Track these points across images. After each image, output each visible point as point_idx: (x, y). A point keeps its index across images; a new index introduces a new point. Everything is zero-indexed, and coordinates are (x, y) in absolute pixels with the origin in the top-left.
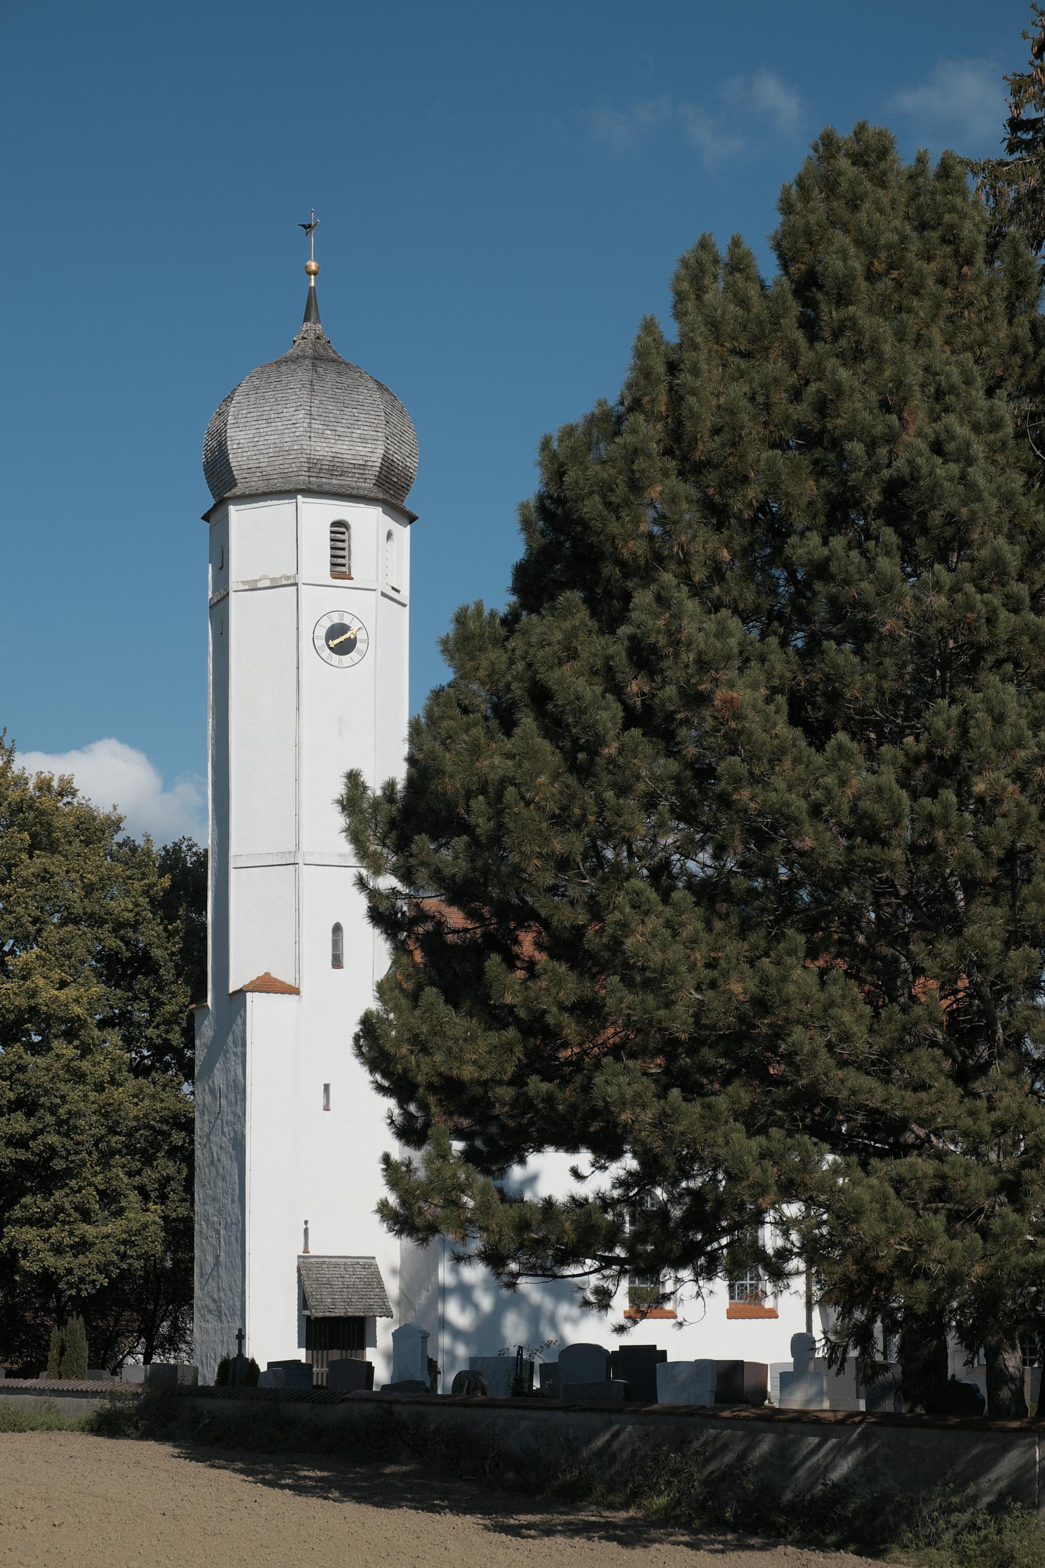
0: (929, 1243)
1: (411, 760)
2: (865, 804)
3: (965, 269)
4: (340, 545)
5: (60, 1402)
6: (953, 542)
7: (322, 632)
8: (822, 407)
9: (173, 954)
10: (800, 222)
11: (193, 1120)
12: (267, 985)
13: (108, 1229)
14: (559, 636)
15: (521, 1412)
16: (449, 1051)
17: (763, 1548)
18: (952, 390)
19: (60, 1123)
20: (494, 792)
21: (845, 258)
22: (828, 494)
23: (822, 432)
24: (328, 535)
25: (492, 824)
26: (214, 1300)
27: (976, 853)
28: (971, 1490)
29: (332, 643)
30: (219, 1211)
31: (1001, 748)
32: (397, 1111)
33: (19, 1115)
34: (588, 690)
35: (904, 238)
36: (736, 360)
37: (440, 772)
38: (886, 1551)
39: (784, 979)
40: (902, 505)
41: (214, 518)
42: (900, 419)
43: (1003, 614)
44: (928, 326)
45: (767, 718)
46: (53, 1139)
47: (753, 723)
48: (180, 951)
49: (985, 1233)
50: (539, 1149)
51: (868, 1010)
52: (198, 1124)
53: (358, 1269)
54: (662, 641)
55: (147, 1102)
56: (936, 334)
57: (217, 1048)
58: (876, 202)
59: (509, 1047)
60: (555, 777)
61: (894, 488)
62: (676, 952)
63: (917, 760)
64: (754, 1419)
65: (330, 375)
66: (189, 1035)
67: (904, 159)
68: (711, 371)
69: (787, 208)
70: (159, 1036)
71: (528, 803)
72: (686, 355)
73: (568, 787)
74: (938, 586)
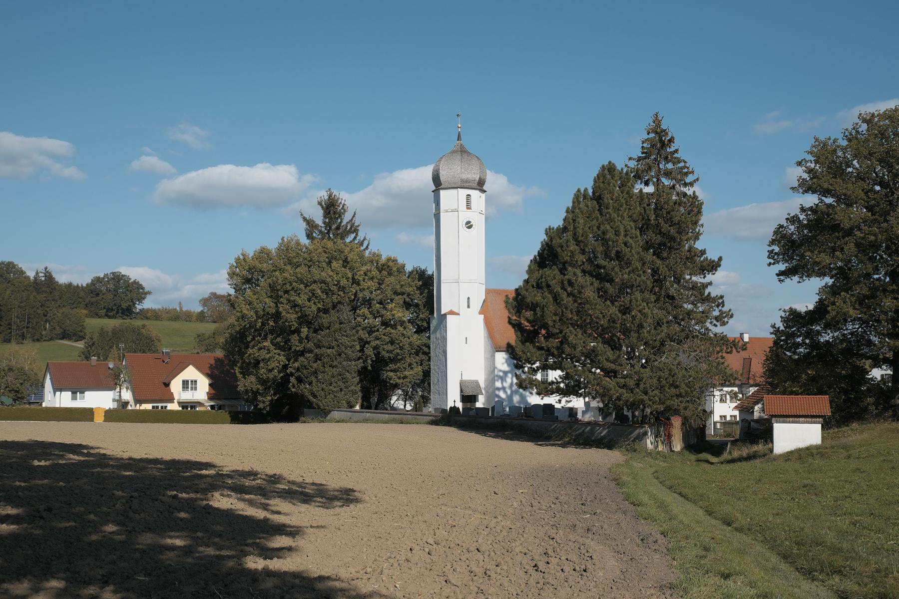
6: (629, 263)
8: (604, 233)
12: (452, 313)
40: (619, 256)
46: (398, 351)
61: (617, 252)
65: (465, 156)
69: (595, 181)
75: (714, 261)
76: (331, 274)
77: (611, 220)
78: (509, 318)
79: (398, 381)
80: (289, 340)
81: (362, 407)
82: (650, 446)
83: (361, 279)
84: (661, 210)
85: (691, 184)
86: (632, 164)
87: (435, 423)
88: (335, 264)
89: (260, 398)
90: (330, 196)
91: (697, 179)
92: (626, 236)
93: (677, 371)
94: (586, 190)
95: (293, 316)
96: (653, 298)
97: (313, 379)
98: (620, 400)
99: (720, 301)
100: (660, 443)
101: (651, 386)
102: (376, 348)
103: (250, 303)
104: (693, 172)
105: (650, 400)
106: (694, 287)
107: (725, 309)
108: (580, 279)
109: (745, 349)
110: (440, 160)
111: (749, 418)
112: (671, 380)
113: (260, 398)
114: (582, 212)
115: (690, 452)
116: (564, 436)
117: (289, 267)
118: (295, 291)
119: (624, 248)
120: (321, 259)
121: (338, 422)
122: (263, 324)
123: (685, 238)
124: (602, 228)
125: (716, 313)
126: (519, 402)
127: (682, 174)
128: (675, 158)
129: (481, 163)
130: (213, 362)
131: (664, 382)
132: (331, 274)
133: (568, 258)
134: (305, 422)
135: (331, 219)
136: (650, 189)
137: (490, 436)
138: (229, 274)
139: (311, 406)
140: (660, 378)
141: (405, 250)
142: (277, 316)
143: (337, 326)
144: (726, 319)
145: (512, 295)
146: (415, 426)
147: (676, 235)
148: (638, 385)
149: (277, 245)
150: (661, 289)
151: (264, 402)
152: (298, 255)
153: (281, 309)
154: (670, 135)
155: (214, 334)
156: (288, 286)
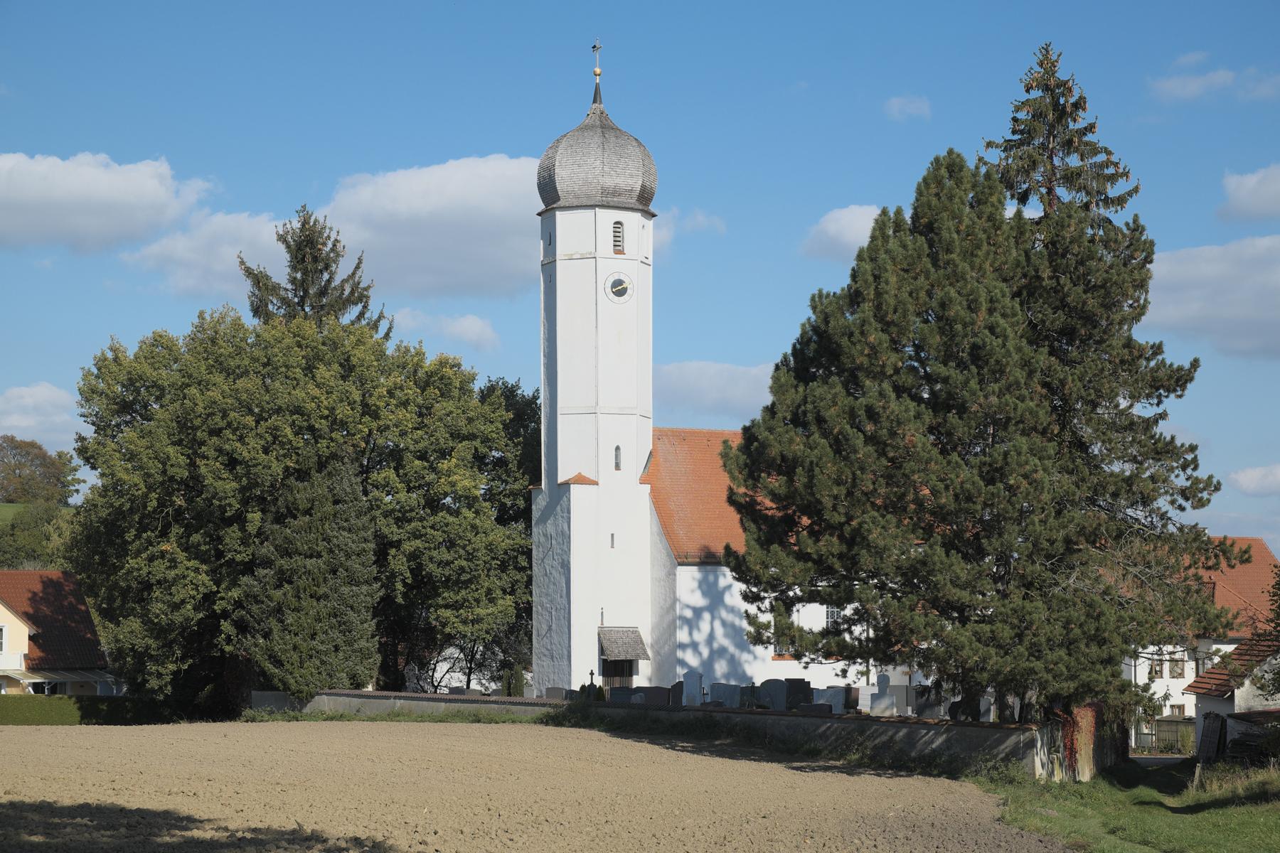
2: (968, 486)
6: (999, 371)
7: (609, 284)
12: (581, 480)
13: (489, 611)
18: (998, 301)
28: (995, 751)
31: (1020, 465)
35: (974, 223)
46: (464, 563)
52: (534, 553)
56: (987, 265)
57: (548, 512)
59: (808, 570)
61: (975, 347)
65: (611, 136)
69: (920, 193)
75: (1180, 369)
76: (316, 392)
78: (730, 489)
79: (461, 628)
80: (220, 539)
81: (379, 687)
83: (382, 404)
84: (1063, 256)
85: (1120, 201)
86: (994, 156)
87: (555, 720)
88: (322, 372)
89: (152, 667)
90: (305, 223)
91: (1136, 190)
92: (991, 311)
94: (899, 212)
95: (229, 486)
97: (273, 623)
98: (983, 669)
99: (1189, 457)
100: (1057, 766)
102: (414, 556)
103: (131, 456)
104: (1126, 174)
105: (1048, 670)
106: (1132, 425)
107: (1202, 473)
108: (894, 405)
109: (1248, 561)
110: (555, 147)
111: (1222, 710)
112: (1091, 627)
113: (152, 667)
114: (893, 259)
115: (1111, 783)
116: (849, 749)
117: (219, 378)
118: (234, 431)
120: (292, 361)
121: (332, 719)
122: (162, 503)
123: (1117, 317)
124: (939, 293)
125: (1180, 481)
126: (727, 676)
127: (1100, 179)
128: (1087, 144)
129: (646, 155)
130: (38, 587)
131: (1077, 631)
132: (316, 392)
133: (865, 361)
134: (253, 720)
135: (305, 273)
136: (1033, 211)
137: (684, 750)
138: (81, 392)
139: (267, 683)
140: (1068, 622)
141: (477, 342)
142: (193, 485)
143: (329, 508)
144: (1205, 495)
145: (737, 442)
146: (508, 727)
147: (1099, 311)
148: (1020, 636)
149: (188, 330)
150: (1063, 428)
151: (160, 675)
152: (239, 351)
153: (203, 470)
155: (13, 527)
156: (217, 419)
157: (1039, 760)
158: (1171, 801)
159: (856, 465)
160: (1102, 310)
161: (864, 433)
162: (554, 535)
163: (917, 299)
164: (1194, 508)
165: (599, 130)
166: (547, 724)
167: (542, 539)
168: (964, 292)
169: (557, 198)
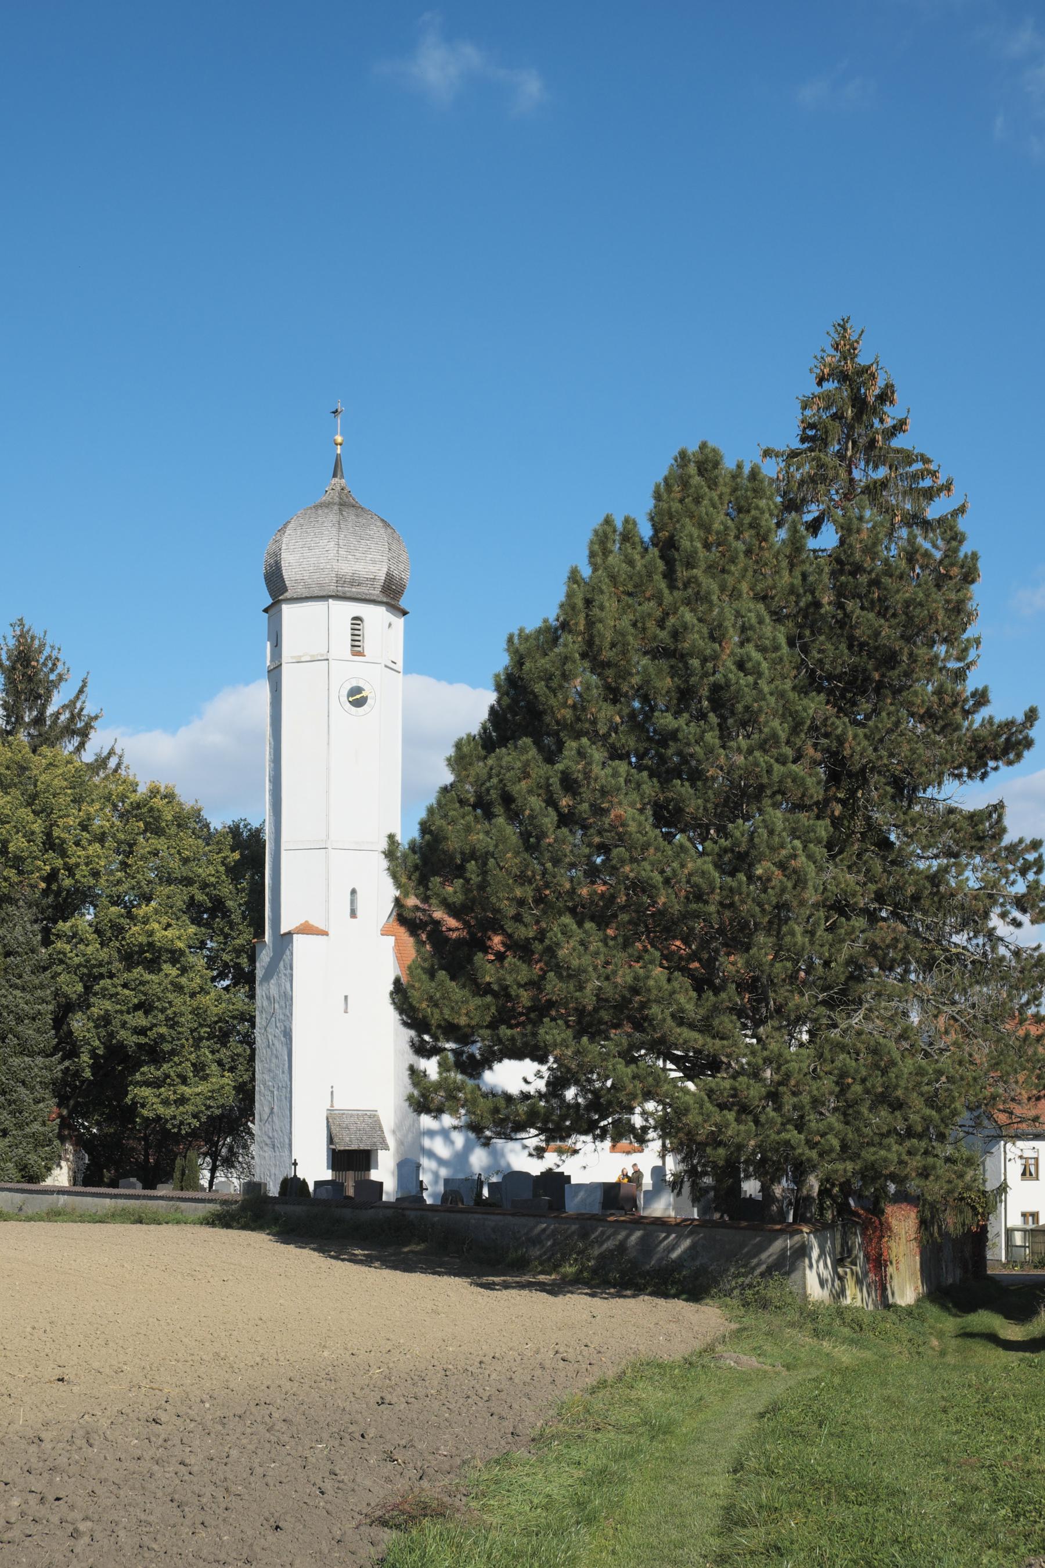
0: (726, 1127)
1: (425, 828)
3: (763, 544)
4: (357, 632)
5: (183, 1205)
6: (749, 720)
8: (675, 635)
9: (240, 905)
10: (665, 506)
11: (255, 1017)
12: (307, 929)
13: (198, 1090)
14: (519, 764)
15: (485, 1216)
16: (453, 1008)
17: (634, 1296)
18: (752, 628)
19: (167, 1019)
20: (481, 857)
21: (692, 541)
22: (678, 687)
23: (675, 650)
24: (349, 626)
25: (480, 878)
26: (269, 1137)
27: (757, 909)
29: (351, 699)
30: (273, 1078)
31: (773, 849)
32: (416, 1039)
33: (140, 1013)
34: (536, 802)
35: (726, 528)
36: (626, 598)
37: (446, 839)
38: (702, 1299)
39: (648, 977)
40: (721, 698)
41: (272, 611)
42: (720, 645)
43: (776, 767)
44: (739, 582)
45: (640, 824)
46: (163, 1030)
47: (633, 827)
48: (246, 903)
49: (757, 1122)
50: (500, 1061)
51: (694, 994)
52: (258, 1020)
53: (366, 1118)
54: (581, 776)
55: (224, 1005)
56: (744, 587)
57: (271, 970)
58: (711, 500)
59: (488, 1007)
60: (517, 854)
61: (716, 688)
62: (586, 960)
63: (725, 851)
64: (630, 1222)
65: (351, 516)
66: (252, 960)
67: (729, 464)
68: (611, 605)
69: (658, 496)
70: (231, 960)
71: (501, 869)
72: (596, 597)
73: (525, 859)
74: (739, 750)
75: (1010, 724)
77: (702, 597)
82: (815, 1292)
93: (896, 1055)
96: (823, 829)
99: (1031, 857)
101: (816, 1102)
105: (811, 1145)
110: (282, 530)
112: (878, 1083)
115: (944, 1307)
116: (564, 1258)
119: (734, 675)
131: (858, 1088)
140: (843, 1075)
154: (881, 382)
157: (814, 1281)
158: (1013, 1332)
159: (547, 855)
160: (902, 643)
161: (556, 808)
162: (277, 996)
163: (644, 629)
164: (1033, 922)
165: (336, 507)
166: (228, 1226)
167: (265, 1003)
168: (708, 618)
169: (285, 589)
